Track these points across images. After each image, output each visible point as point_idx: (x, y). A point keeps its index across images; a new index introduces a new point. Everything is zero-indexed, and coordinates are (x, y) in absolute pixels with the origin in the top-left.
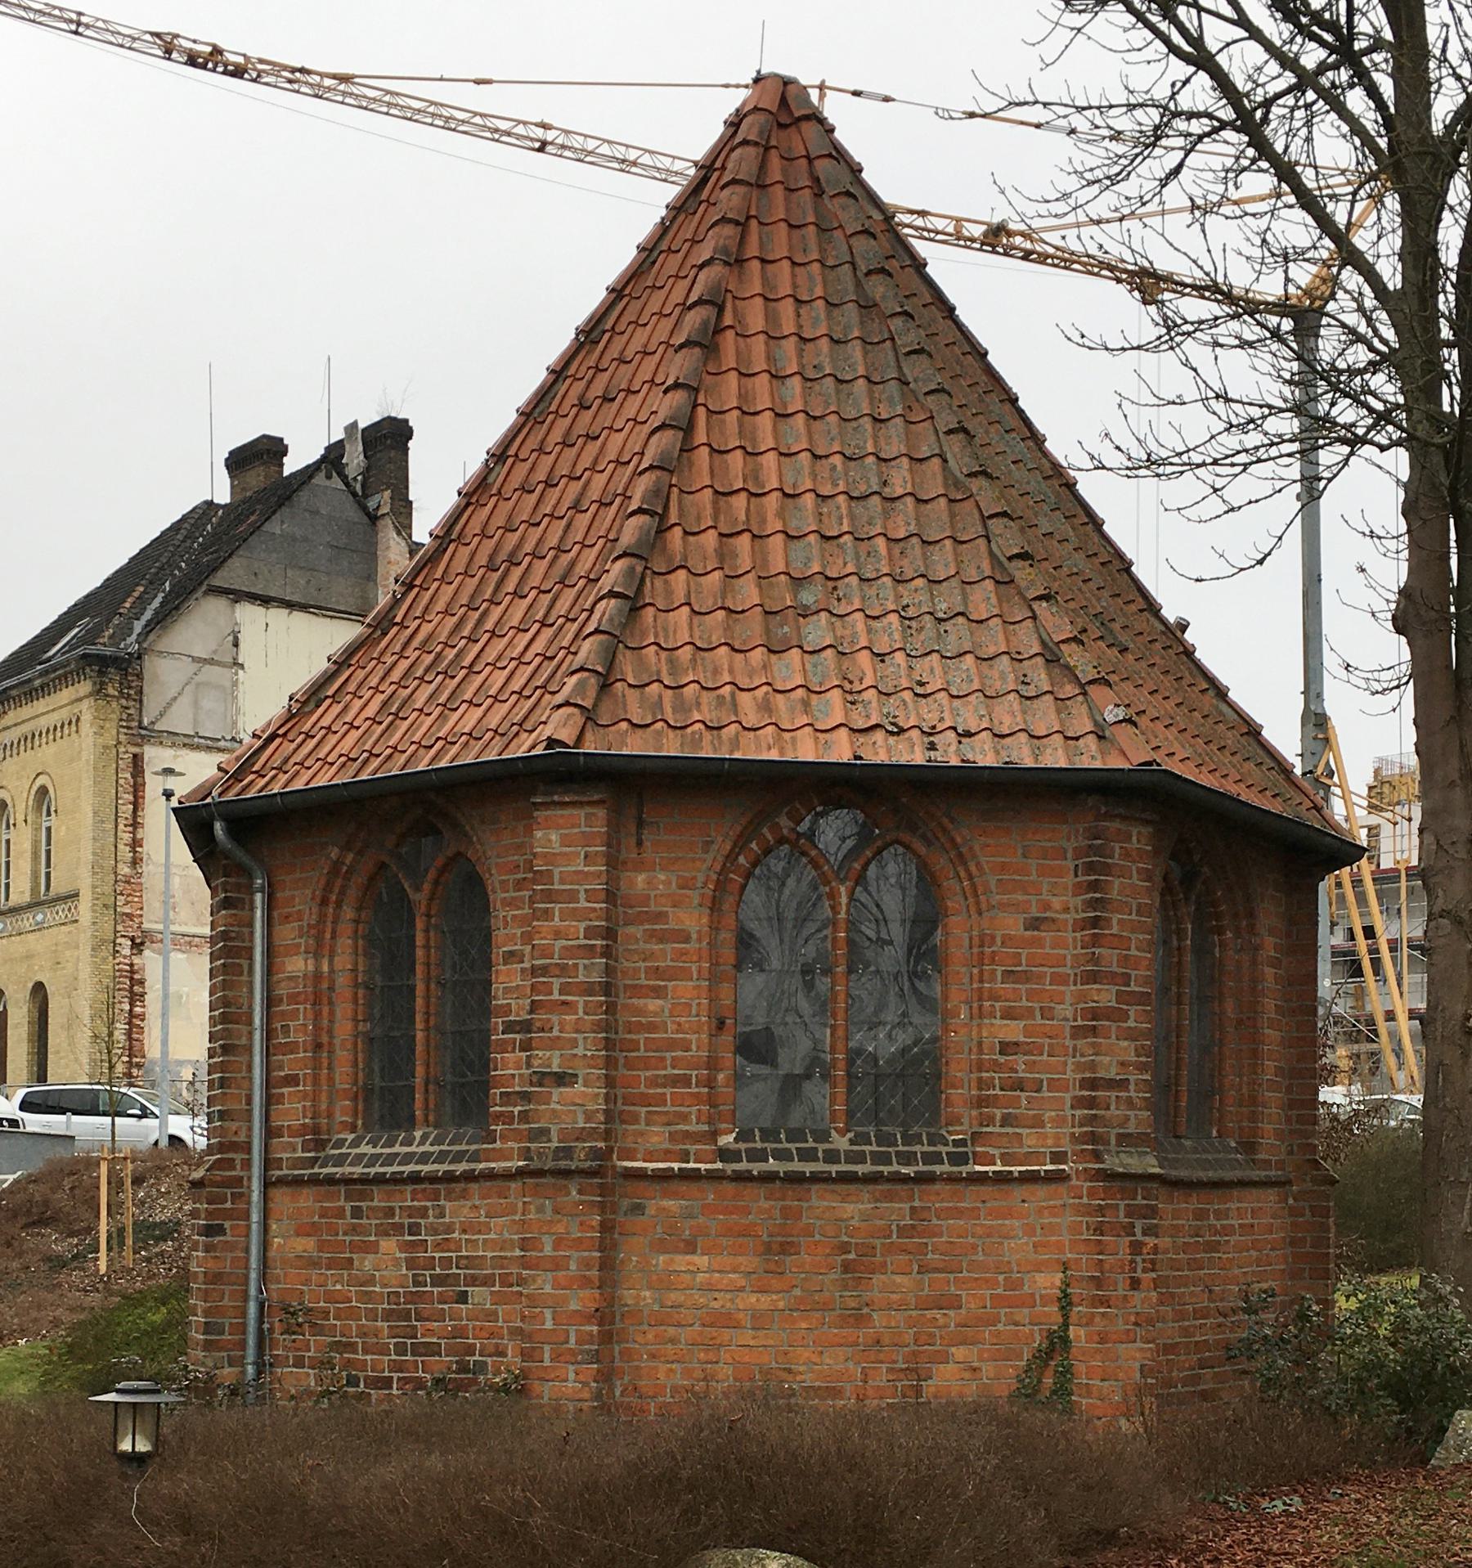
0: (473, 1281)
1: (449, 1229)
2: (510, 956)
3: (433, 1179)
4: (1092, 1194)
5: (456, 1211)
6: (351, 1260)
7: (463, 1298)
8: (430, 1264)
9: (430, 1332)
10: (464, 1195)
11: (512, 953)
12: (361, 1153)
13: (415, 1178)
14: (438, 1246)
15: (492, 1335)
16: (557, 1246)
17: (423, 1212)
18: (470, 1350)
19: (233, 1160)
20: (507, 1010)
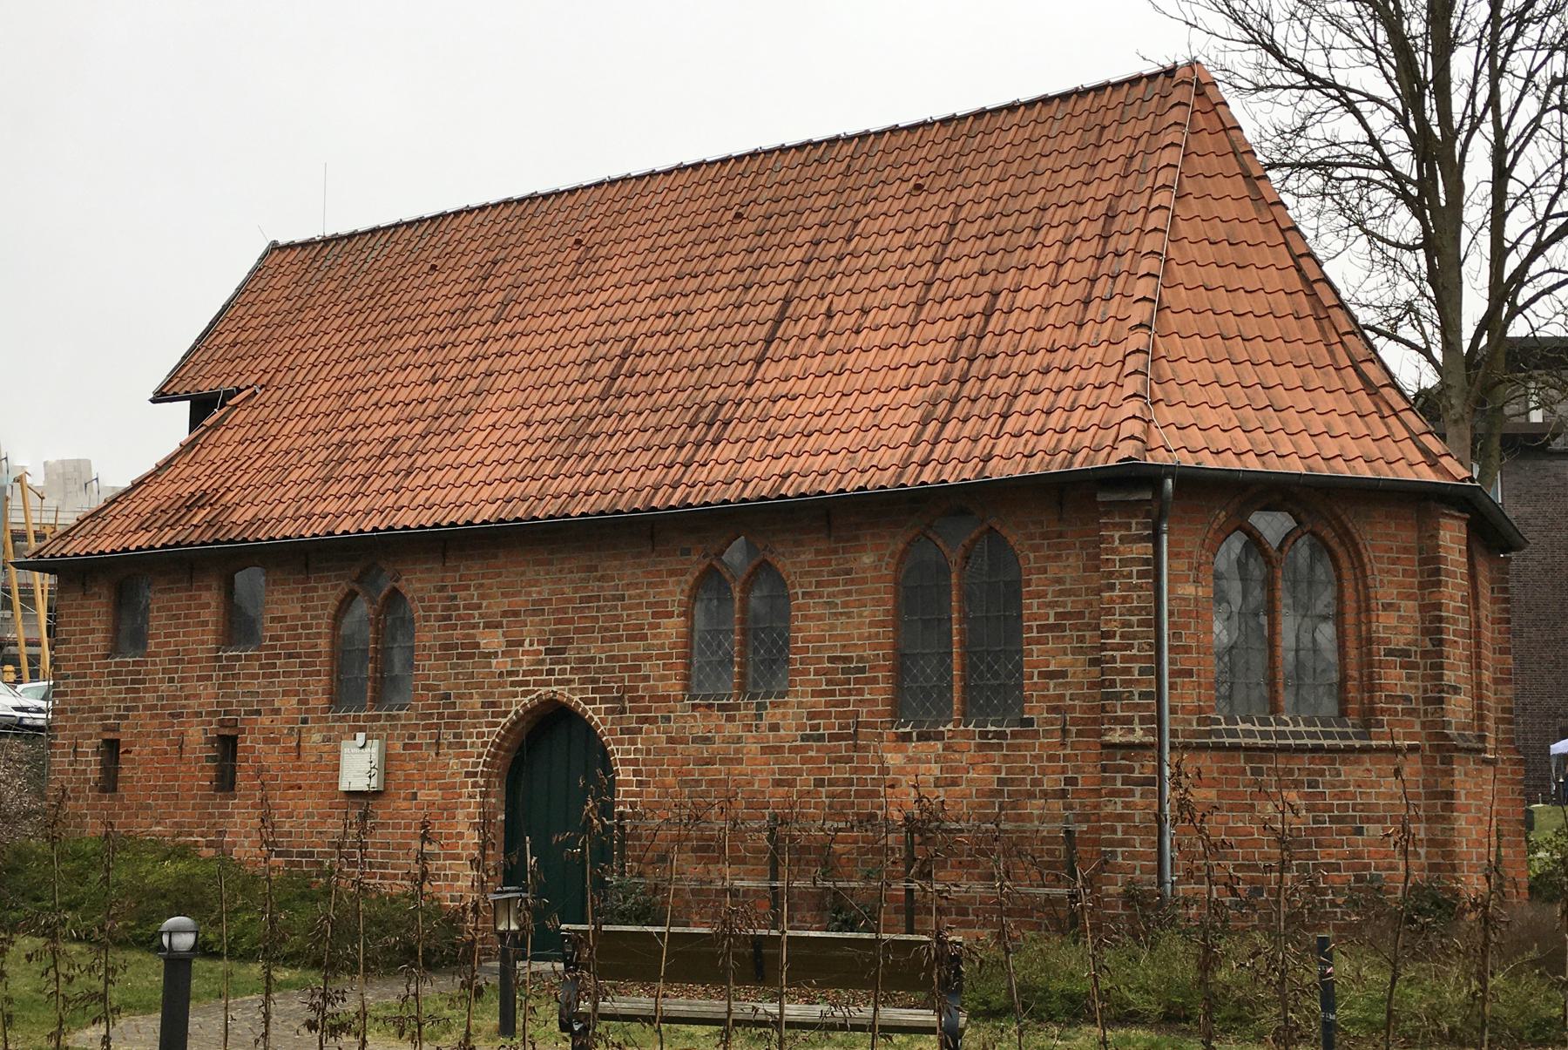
0: (1368, 820)
1: (1346, 784)
2: (1387, 607)
3: (1331, 750)
4: (1514, 772)
5: (1350, 773)
6: (1253, 806)
7: (1359, 831)
8: (1330, 808)
9: (1330, 855)
10: (1358, 762)
11: (1390, 605)
12: (1248, 731)
13: (1317, 749)
14: (1337, 796)
15: (1386, 856)
16: (1125, 832)
17: (1322, 773)
18: (1367, 867)
19: (29, 656)
20: (1388, 641)
